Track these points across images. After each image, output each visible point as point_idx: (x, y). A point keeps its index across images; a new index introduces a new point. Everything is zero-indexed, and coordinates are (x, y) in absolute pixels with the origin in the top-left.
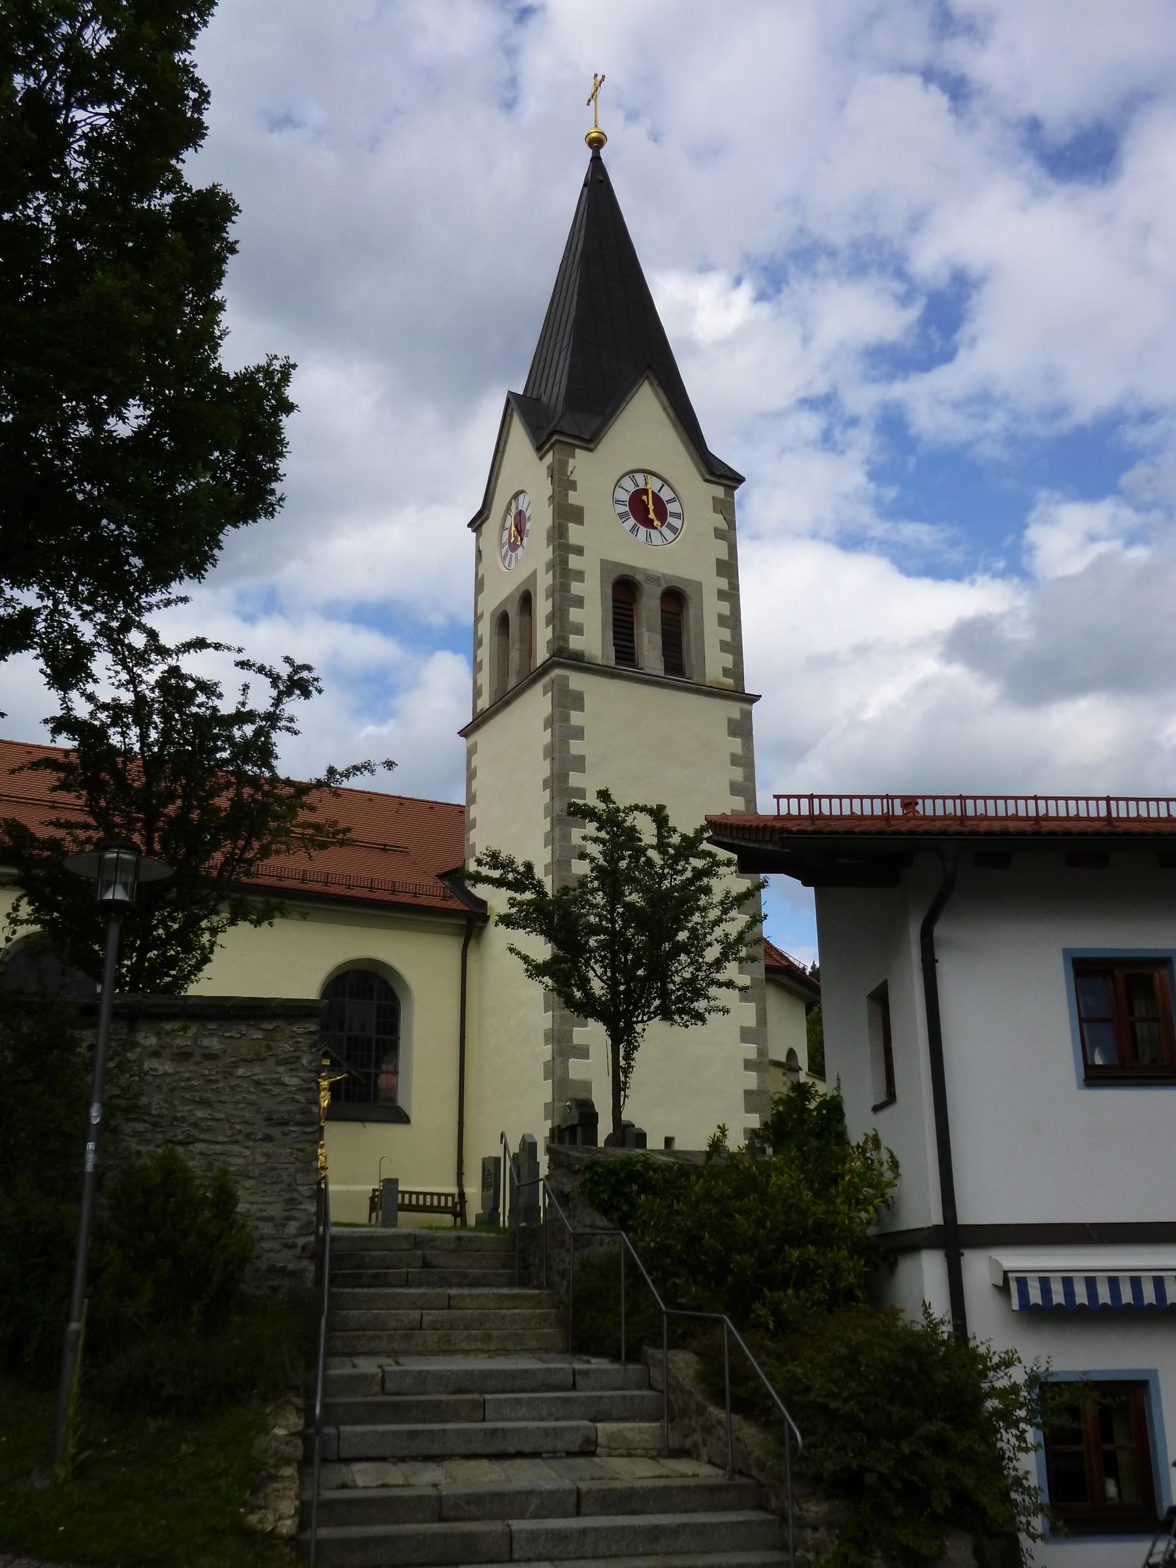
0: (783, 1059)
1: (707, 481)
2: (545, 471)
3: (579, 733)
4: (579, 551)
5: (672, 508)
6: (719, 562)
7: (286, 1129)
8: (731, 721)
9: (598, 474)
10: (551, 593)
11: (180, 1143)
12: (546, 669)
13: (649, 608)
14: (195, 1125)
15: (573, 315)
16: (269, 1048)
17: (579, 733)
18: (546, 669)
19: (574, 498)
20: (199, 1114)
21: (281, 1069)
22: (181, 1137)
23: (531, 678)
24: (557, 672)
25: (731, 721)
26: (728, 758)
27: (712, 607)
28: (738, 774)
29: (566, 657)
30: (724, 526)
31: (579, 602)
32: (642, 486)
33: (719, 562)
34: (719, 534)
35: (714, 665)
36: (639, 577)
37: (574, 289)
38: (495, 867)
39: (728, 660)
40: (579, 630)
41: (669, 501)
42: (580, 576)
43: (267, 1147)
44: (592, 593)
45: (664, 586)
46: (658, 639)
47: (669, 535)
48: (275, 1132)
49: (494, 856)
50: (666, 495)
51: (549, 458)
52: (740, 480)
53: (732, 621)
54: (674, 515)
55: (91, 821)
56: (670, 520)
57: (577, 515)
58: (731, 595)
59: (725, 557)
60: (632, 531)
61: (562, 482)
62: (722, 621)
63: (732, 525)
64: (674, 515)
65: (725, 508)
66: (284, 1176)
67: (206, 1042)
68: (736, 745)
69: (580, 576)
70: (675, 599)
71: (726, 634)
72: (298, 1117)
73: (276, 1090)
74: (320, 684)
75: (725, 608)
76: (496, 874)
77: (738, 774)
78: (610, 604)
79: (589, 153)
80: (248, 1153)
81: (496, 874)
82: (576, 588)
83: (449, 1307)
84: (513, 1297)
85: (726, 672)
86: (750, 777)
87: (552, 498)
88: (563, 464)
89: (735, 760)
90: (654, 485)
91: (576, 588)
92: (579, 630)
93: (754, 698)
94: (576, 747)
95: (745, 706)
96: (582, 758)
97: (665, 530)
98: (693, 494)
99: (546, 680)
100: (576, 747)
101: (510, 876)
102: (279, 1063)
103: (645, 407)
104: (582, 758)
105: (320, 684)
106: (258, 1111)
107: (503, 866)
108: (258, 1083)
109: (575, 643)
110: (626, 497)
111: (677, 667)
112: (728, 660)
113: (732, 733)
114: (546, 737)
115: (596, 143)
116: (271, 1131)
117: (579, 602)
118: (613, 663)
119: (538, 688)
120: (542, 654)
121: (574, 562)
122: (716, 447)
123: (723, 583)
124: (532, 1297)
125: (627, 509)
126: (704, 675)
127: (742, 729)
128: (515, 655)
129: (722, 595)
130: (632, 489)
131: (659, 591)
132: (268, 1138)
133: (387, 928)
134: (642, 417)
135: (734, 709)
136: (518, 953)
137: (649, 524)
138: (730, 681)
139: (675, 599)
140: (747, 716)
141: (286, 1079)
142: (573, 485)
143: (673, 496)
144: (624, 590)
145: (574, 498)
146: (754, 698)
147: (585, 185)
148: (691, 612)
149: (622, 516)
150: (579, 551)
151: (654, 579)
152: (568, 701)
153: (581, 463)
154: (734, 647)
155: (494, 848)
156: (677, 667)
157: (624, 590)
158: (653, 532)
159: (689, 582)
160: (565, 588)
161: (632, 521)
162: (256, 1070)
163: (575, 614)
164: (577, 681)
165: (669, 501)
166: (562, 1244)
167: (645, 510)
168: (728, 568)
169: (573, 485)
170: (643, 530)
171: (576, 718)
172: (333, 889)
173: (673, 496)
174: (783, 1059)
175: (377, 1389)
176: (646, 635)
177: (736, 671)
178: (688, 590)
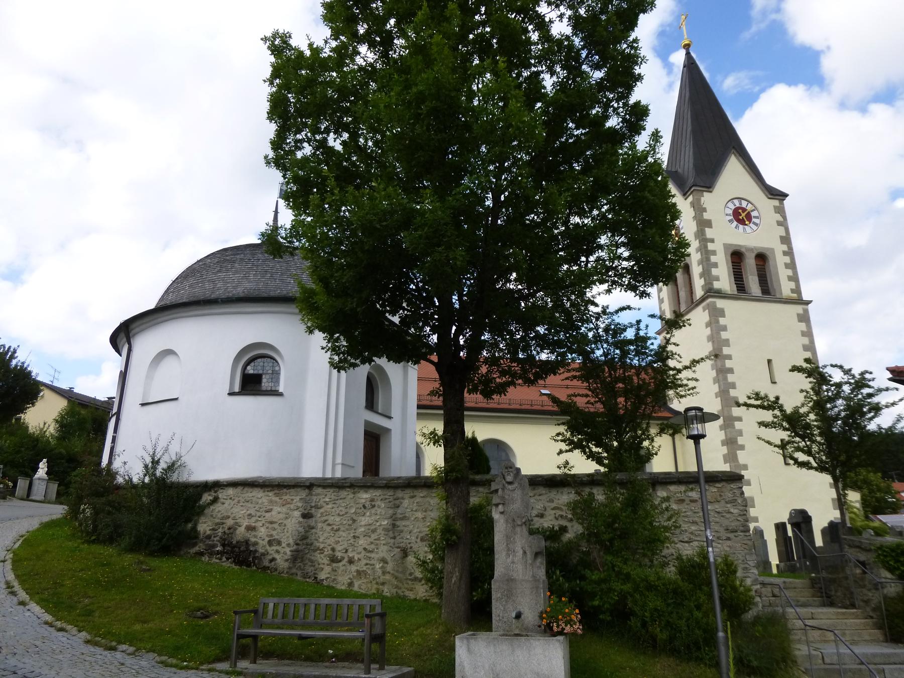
2: (689, 205)
3: (724, 328)
4: (712, 241)
5: (754, 214)
6: (781, 237)
7: (736, 534)
8: (798, 315)
10: (700, 262)
11: (686, 542)
12: (703, 299)
13: (750, 263)
14: (692, 533)
15: (689, 129)
16: (721, 496)
17: (724, 328)
18: (703, 299)
19: (706, 216)
20: (693, 528)
21: (729, 505)
22: (686, 539)
23: (694, 304)
24: (710, 300)
25: (798, 315)
26: (800, 333)
27: (780, 260)
28: (806, 341)
29: (711, 292)
30: (781, 219)
31: (716, 265)
33: (781, 237)
34: (779, 224)
35: (786, 288)
36: (743, 250)
37: (688, 115)
38: (757, 400)
39: (792, 285)
40: (717, 279)
42: (714, 253)
43: (728, 543)
44: (722, 261)
45: (756, 252)
46: (756, 279)
47: (754, 227)
48: (731, 535)
49: (757, 394)
50: (749, 208)
51: (690, 198)
52: (787, 195)
53: (792, 265)
54: (755, 217)
55: (590, 393)
56: (754, 220)
57: (709, 223)
58: (789, 253)
59: (784, 234)
61: (699, 209)
62: (787, 266)
63: (785, 218)
64: (755, 217)
65: (780, 210)
66: (740, 556)
67: (690, 494)
68: (803, 327)
69: (714, 253)
70: (762, 258)
71: (790, 272)
72: (742, 528)
73: (728, 516)
74: (691, 322)
75: (787, 259)
76: (758, 402)
77: (806, 341)
78: (730, 264)
80: (719, 546)
81: (758, 402)
82: (713, 259)
83: (813, 618)
84: (843, 614)
85: (793, 291)
86: (812, 342)
87: (695, 218)
88: (699, 200)
89: (803, 334)
90: (744, 204)
91: (713, 259)
92: (717, 279)
93: (808, 303)
94: (724, 335)
95: (805, 307)
96: (728, 340)
97: (751, 225)
98: (764, 206)
99: (704, 304)
100: (724, 335)
101: (766, 404)
102: (727, 503)
103: (733, 165)
104: (728, 340)
105: (691, 322)
106: (721, 526)
107: (762, 399)
108: (718, 513)
109: (716, 285)
110: (731, 212)
111: (768, 291)
112: (792, 285)
113: (800, 321)
114: (708, 331)
116: (729, 535)
117: (716, 265)
118: (736, 293)
119: (700, 308)
120: (699, 293)
121: (711, 246)
122: (769, 181)
123: (785, 247)
124: (853, 613)
126: (781, 294)
127: (804, 318)
128: (683, 294)
129: (785, 253)
130: (733, 208)
131: (753, 255)
132: (728, 539)
134: (732, 173)
135: (799, 309)
138: (795, 295)
139: (762, 258)
140: (806, 312)
141: (732, 510)
142: (705, 210)
144: (736, 257)
145: (706, 216)
146: (808, 303)
147: (684, 67)
148: (771, 262)
149: (730, 221)
150: (712, 241)
151: (751, 250)
152: (716, 314)
153: (707, 199)
154: (795, 278)
155: (757, 390)
156: (768, 291)
157: (736, 257)
159: (768, 249)
160: (708, 259)
161: (735, 223)
162: (717, 506)
163: (714, 272)
164: (720, 303)
166: (864, 586)
167: (741, 216)
168: (786, 240)
169: (705, 210)
170: (741, 226)
171: (722, 321)
172: (535, 408)
175: (820, 661)
176: (750, 277)
177: (797, 290)
178: (768, 253)
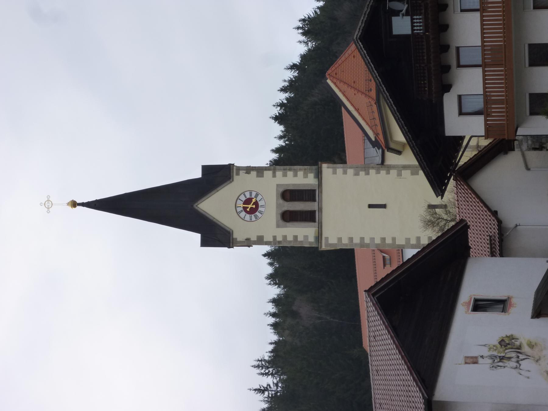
0: (271, 240)
1: (233, 180)
9: (239, 226)
19: (254, 238)
32: (242, 209)
41: (246, 197)
60: (261, 214)
79: (79, 208)
110: (248, 216)
115: (74, 204)
125: (253, 215)
133: (204, 213)
136: (80, 204)
137: (256, 203)
143: (242, 195)
151: (278, 206)
157: (288, 217)
158: (258, 200)
161: (257, 213)
165: (246, 197)
173: (242, 195)
174: (271, 240)
